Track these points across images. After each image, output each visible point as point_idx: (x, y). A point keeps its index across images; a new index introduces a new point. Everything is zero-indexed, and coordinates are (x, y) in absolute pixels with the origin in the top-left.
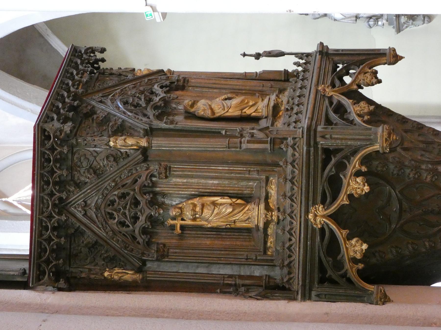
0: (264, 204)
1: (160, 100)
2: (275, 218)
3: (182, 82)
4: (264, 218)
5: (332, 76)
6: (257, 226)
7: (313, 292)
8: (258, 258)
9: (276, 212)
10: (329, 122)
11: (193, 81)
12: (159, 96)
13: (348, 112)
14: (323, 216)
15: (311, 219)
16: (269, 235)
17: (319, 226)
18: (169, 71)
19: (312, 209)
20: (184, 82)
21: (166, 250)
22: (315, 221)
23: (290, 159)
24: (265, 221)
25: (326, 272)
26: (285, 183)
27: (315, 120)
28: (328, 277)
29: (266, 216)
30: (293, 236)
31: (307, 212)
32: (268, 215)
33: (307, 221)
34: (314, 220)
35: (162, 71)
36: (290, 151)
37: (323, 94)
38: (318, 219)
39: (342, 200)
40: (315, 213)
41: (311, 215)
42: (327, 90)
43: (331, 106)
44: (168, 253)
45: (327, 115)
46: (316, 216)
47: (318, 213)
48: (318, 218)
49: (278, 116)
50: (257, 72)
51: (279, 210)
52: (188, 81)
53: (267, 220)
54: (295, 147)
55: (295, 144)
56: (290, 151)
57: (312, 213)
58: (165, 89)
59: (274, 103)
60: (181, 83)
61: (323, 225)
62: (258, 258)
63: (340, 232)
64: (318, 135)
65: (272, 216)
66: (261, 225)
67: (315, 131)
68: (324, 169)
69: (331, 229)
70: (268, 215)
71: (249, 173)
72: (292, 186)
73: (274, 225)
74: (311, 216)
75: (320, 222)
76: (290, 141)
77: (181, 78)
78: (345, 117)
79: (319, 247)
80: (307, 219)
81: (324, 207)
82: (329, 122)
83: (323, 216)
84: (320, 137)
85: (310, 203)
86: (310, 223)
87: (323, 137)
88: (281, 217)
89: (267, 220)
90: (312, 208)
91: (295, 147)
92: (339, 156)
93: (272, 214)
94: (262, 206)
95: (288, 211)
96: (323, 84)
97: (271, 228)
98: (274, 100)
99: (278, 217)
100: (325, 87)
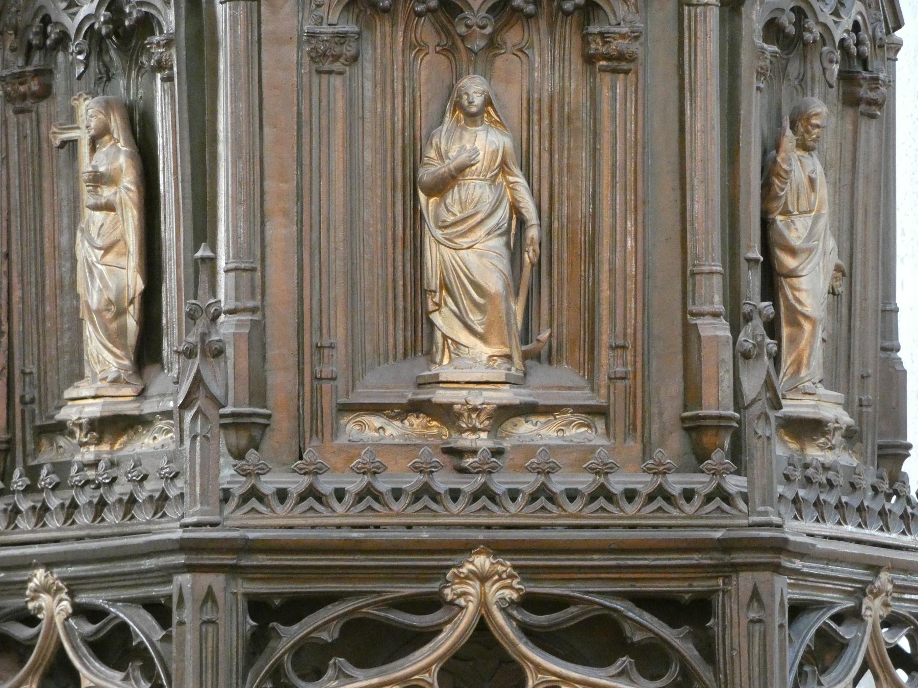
0: (517, 402)
1: (825, 26)
2: (467, 440)
3: (872, 95)
4: (467, 403)
5: (912, 618)
6: (436, 382)
7: (188, 576)
8: (326, 386)
9: (491, 444)
10: (797, 610)
11: (869, 130)
12: (835, 22)
13: (822, 679)
14: (483, 603)
15: (472, 563)
16: (402, 421)
17: (449, 594)
18: (897, 46)
19: (505, 566)
20: (872, 103)
21: (337, 66)
22: (467, 577)
23: (676, 483)
24: (456, 407)
25: (289, 622)
26: (531, 470)
27: (804, 566)
28: (274, 628)
29: (475, 409)
30: (586, 505)
31: (497, 549)
32: (478, 416)
33: (467, 548)
34: (471, 571)
35: (899, 24)
36: (701, 482)
37: (867, 590)
38: (472, 588)
39: (539, 668)
40: (494, 575)
41: (487, 564)
42: (878, 602)
43: (834, 618)
44: (330, 72)
45: (818, 606)
46: (483, 578)
47: (493, 584)
48: (477, 584)
49: (786, 438)
50: (898, 350)
51: (498, 452)
52: (873, 116)
53: (459, 416)
54: (543, 498)
55: (377, 499)
56: (701, 482)
57: (492, 564)
58: (851, 41)
59: (828, 422)
60: (864, 92)
61: (452, 603)
62: (326, 386)
63: (429, 665)
64: (762, 576)
65: (474, 430)
66: (441, 396)
67: (777, 569)
68: (643, 601)
69: (440, 632)
70: (478, 416)
71: (617, 347)
72: (583, 495)
73: (439, 436)
74: (482, 562)
75: (464, 594)
76: (734, 483)
77: (883, 89)
78: (807, 668)
79: (379, 593)
80: (471, 550)
81: (512, 602)
82: (797, 610)
83: (483, 603)
84: (755, 584)
85: (71, 570)
86: (458, 558)
87: (755, 595)
88: (468, 461)
89: (459, 416)
90: (508, 563)
91: (543, 498)
92: (689, 650)
93: (483, 430)
94: (507, 395)
95: (500, 484)
96: (895, 586)
97: (427, 428)
98: (837, 422)
99: (474, 452)
100: (887, 595)
